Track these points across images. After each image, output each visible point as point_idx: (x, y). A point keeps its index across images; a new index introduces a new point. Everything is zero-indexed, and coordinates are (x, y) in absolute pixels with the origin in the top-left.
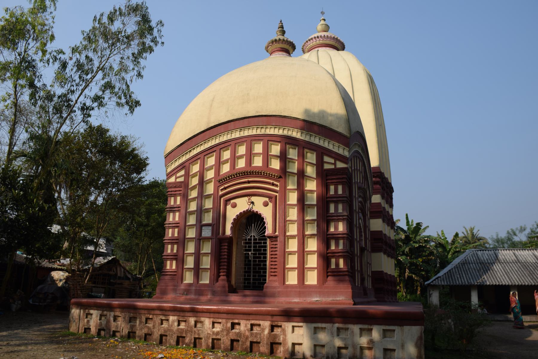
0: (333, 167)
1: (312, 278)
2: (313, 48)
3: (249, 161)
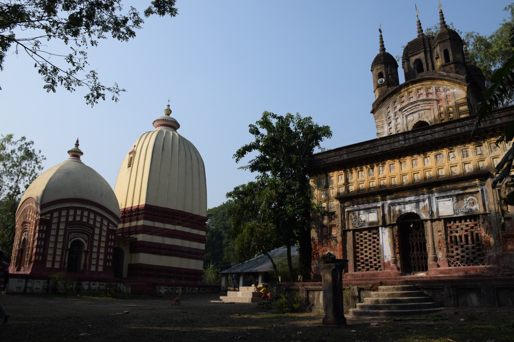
0: (112, 228)
1: (100, 269)
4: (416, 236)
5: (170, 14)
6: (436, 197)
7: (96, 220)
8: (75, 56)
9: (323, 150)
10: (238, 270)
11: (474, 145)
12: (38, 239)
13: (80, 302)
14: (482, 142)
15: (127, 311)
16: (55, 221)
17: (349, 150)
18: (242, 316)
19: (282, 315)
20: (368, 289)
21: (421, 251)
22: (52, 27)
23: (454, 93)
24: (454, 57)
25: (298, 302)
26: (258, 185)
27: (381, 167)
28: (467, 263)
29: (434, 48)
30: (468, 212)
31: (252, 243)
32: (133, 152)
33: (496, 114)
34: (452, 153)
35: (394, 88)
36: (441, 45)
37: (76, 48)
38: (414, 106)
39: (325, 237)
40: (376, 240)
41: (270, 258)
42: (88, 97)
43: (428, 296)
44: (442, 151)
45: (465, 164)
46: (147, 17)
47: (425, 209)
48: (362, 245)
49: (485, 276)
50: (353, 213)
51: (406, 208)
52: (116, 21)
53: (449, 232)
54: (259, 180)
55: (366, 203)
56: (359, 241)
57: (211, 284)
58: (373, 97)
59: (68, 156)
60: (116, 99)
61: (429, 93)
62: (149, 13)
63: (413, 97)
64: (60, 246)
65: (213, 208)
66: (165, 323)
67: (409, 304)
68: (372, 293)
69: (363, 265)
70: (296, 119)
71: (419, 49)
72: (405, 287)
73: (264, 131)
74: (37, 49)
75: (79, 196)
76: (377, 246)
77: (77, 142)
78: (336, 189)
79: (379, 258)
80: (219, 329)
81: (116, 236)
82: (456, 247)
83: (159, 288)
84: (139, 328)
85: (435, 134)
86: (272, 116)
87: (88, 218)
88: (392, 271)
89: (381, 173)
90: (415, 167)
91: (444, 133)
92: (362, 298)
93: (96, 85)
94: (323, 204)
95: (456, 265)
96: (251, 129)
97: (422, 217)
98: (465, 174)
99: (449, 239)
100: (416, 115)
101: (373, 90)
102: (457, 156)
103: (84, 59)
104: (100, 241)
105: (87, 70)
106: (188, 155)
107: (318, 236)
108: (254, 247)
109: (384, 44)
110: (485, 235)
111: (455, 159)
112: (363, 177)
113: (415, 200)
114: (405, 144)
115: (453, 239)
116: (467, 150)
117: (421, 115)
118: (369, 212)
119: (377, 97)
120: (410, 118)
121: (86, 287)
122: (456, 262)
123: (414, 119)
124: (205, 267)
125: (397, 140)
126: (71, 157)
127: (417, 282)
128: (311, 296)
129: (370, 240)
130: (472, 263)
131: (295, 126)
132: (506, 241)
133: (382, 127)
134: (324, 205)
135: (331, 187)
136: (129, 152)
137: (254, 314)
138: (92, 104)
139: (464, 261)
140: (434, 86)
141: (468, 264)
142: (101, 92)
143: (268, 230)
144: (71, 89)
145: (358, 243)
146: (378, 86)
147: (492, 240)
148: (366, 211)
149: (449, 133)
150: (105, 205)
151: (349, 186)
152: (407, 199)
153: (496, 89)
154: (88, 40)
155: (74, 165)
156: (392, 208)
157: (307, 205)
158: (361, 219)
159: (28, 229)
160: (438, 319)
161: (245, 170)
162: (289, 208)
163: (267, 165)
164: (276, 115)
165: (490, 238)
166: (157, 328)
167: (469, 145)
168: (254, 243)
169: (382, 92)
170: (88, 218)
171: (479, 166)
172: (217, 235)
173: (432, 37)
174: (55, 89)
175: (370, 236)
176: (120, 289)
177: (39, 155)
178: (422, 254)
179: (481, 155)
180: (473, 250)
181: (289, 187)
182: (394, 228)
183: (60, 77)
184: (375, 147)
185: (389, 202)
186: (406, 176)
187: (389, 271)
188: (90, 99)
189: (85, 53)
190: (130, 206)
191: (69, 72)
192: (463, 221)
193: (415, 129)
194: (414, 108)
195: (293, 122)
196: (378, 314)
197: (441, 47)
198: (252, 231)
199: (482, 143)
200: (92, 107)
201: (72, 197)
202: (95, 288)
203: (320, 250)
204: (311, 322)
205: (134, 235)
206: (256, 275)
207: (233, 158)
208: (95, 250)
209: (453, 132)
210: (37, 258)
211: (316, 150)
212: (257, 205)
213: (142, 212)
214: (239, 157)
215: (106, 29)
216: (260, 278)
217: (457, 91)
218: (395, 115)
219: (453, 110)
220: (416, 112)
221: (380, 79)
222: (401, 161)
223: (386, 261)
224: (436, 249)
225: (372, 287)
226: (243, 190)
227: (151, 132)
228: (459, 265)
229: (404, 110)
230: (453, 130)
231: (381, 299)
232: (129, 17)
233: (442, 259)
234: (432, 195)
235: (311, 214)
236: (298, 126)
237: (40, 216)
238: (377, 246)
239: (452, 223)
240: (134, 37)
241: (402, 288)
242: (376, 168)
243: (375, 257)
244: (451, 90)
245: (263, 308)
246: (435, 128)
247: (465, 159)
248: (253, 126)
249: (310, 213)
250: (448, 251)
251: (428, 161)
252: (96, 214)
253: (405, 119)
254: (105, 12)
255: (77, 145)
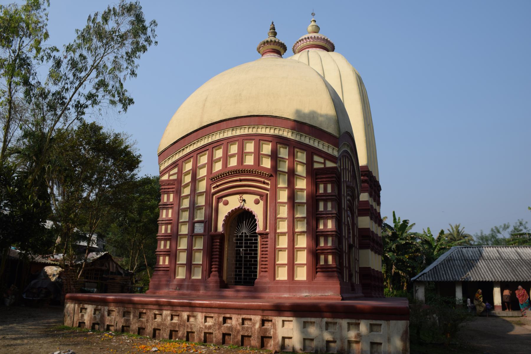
0: (322, 166)
2: (304, 48)
3: (241, 160)
43: (460, 244)
201: (203, 129)
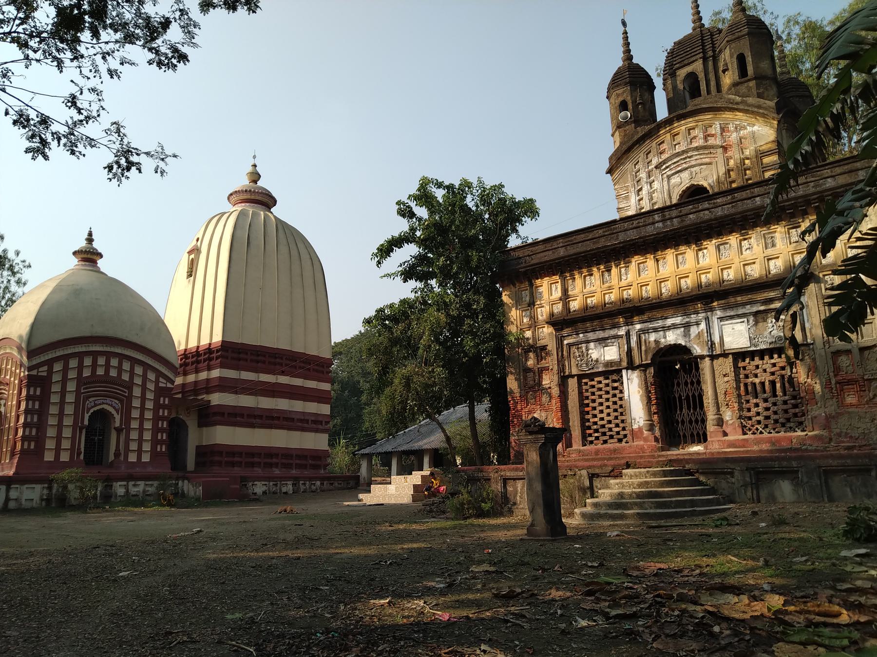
0: (164, 385)
1: (146, 458)
3: (94, 371)
4: (686, 384)
5: (246, 8)
6: (718, 317)
7: (147, 378)
8: (80, 97)
9: (524, 240)
10: (388, 448)
11: (785, 226)
12: (27, 412)
13: (112, 518)
14: (800, 221)
15: (198, 529)
16: (56, 378)
17: (569, 241)
18: (396, 527)
19: (462, 522)
20: (606, 474)
21: (695, 409)
22: (29, 40)
23: (753, 133)
24: (756, 68)
25: (489, 500)
26: (416, 303)
27: (623, 267)
28: (774, 429)
29: (720, 51)
30: (775, 341)
31: (409, 402)
32: (196, 251)
33: (825, 171)
34: (746, 242)
35: (647, 128)
36: (733, 45)
37: (81, 81)
38: (682, 159)
39: (531, 388)
40: (617, 392)
41: (440, 425)
42: (110, 168)
44: (728, 238)
45: (768, 260)
46: (204, 15)
47: (699, 339)
48: (594, 401)
49: (806, 450)
50: (577, 347)
51: (667, 337)
52: (148, 24)
53: (741, 376)
54: (417, 295)
55: (600, 330)
56: (588, 394)
57: (342, 473)
58: (610, 144)
59: (74, 261)
60: (161, 172)
61: (709, 135)
62: (209, 7)
63: (679, 143)
64: (68, 421)
65: (343, 341)
66: (266, 545)
67: (674, 499)
68: (613, 481)
69: (596, 435)
70: (478, 188)
71: (693, 54)
72: (668, 470)
73: (422, 212)
74: (7, 83)
75: (100, 331)
76: (619, 403)
77: (90, 234)
78: (548, 308)
79: (623, 421)
80: (356, 551)
81: (172, 399)
82: (755, 401)
83: (253, 485)
84: (222, 556)
85: (717, 209)
86: (436, 184)
87: (120, 369)
88: (647, 443)
89: (624, 277)
90: (681, 267)
91: (732, 206)
92: (596, 490)
93: (124, 146)
94: (527, 332)
95: (756, 431)
96: (400, 209)
97: (695, 351)
98: (770, 276)
99: (742, 388)
100: (685, 175)
101: (611, 132)
102: (755, 246)
103: (98, 102)
104: (143, 409)
105: (106, 121)
106: (294, 252)
107: (519, 386)
108: (412, 408)
109: (631, 47)
110: (806, 380)
111: (752, 251)
112: (594, 286)
113: (683, 323)
114: (664, 227)
115: (750, 388)
116: (773, 235)
117: (694, 173)
118: (604, 345)
119: (618, 144)
120: (675, 180)
121: (121, 491)
122: (755, 428)
123: (682, 181)
124: (332, 444)
125: (651, 220)
126: (80, 263)
127: (688, 461)
128: (510, 489)
129: (607, 393)
130: (783, 429)
131: (475, 200)
132: (842, 390)
133: (627, 198)
134: (528, 334)
135: (538, 305)
136: (188, 250)
137: (415, 522)
138: (119, 180)
139: (769, 426)
140: (717, 123)
141: (777, 430)
142: (134, 159)
143: (435, 379)
144: (77, 154)
145: (587, 398)
146: (619, 126)
147: (818, 388)
148: (600, 344)
149: (741, 207)
150: (150, 345)
151: (569, 301)
152: (669, 322)
153: (805, 141)
154: (103, 68)
155: (86, 277)
156: (644, 338)
157: (500, 335)
158: (591, 357)
159: (5, 395)
160: (721, 524)
161: (394, 278)
162: (469, 343)
163: (431, 270)
164: (443, 182)
165: (815, 385)
166: (252, 554)
167: (776, 227)
168: (412, 401)
169: (625, 135)
170: (120, 369)
171: (794, 263)
172: (351, 388)
173: (719, 29)
174: (48, 154)
175: (607, 385)
176: (183, 491)
177: (18, 260)
178: (697, 414)
179: (798, 243)
180: (785, 407)
181: (467, 306)
182: (648, 372)
183: (56, 133)
184: (613, 234)
185: (638, 327)
186: (666, 283)
187: (642, 443)
188: (114, 171)
189: (99, 91)
190: (195, 344)
191: (70, 122)
192: (766, 358)
193: (682, 201)
194: (683, 162)
195: (472, 194)
196: (622, 517)
197: (733, 50)
198: (408, 382)
199: (800, 223)
200: (119, 185)
201: (88, 334)
202: (137, 491)
203: (524, 410)
204: (510, 533)
205: (204, 396)
206: (419, 454)
207: (371, 259)
208: (135, 425)
209: (749, 205)
210: (26, 447)
211: (513, 242)
212: (414, 339)
213: (205, 357)
214: (382, 257)
215: (130, 38)
216: (426, 460)
217: (760, 129)
218: (649, 177)
219: (751, 164)
220: (686, 169)
221: (623, 114)
222: (657, 257)
223: (635, 427)
224: (720, 405)
225: (613, 471)
226: (391, 313)
227: (225, 213)
228: (761, 431)
229: (664, 167)
230: (749, 201)
231: (627, 491)
232: (172, 17)
233: (731, 422)
234: (712, 314)
235: (506, 351)
236: (481, 200)
237: (28, 372)
238: (619, 403)
239: (747, 360)
240: (187, 63)
241: (662, 472)
242: (614, 270)
243: (617, 421)
244: (748, 127)
245: (431, 511)
246: (715, 199)
247: (770, 252)
248: (404, 204)
249: (504, 348)
250: (741, 409)
251: (704, 256)
252: (134, 361)
253: (665, 183)
254: (127, 8)
255: (90, 240)
